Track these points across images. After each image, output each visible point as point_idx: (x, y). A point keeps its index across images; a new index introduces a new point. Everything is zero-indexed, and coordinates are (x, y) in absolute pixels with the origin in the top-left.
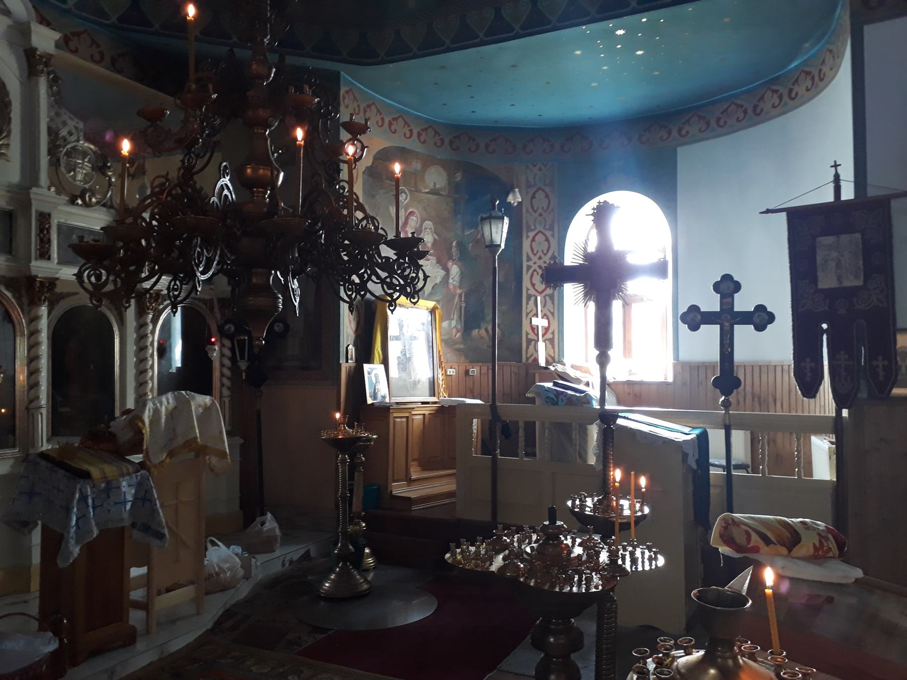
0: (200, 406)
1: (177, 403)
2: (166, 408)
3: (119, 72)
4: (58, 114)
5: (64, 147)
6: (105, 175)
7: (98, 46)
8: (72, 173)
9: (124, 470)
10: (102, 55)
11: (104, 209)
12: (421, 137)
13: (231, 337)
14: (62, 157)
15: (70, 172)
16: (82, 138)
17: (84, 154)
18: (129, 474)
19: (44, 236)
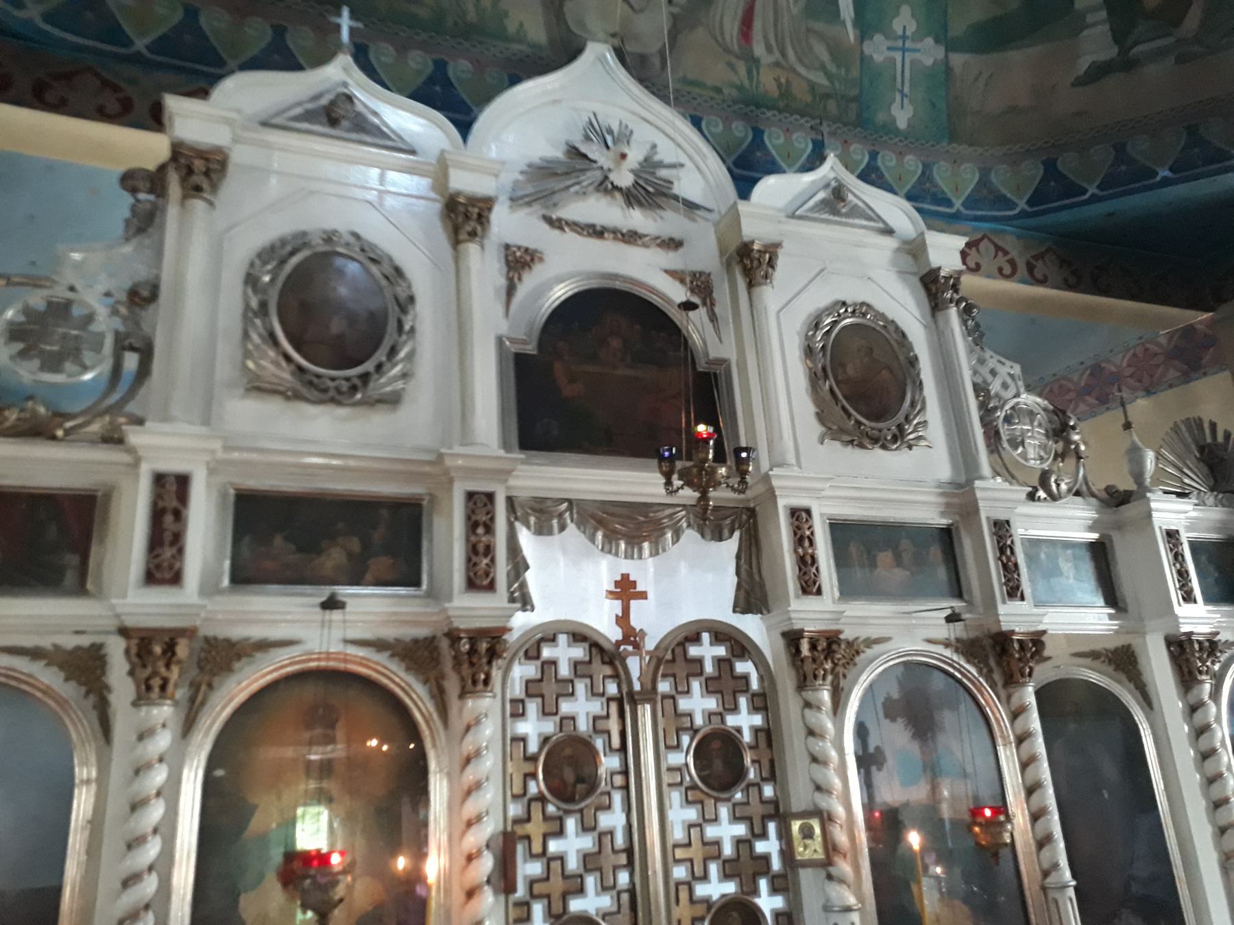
1: (231, 660)
3: (1042, 282)
4: (982, 361)
5: (1002, 408)
7: (1006, 253)
8: (1020, 450)
10: (1012, 263)
11: (1079, 499)
14: (1000, 425)
15: (1016, 448)
16: (1022, 390)
17: (1031, 414)
19: (1009, 559)
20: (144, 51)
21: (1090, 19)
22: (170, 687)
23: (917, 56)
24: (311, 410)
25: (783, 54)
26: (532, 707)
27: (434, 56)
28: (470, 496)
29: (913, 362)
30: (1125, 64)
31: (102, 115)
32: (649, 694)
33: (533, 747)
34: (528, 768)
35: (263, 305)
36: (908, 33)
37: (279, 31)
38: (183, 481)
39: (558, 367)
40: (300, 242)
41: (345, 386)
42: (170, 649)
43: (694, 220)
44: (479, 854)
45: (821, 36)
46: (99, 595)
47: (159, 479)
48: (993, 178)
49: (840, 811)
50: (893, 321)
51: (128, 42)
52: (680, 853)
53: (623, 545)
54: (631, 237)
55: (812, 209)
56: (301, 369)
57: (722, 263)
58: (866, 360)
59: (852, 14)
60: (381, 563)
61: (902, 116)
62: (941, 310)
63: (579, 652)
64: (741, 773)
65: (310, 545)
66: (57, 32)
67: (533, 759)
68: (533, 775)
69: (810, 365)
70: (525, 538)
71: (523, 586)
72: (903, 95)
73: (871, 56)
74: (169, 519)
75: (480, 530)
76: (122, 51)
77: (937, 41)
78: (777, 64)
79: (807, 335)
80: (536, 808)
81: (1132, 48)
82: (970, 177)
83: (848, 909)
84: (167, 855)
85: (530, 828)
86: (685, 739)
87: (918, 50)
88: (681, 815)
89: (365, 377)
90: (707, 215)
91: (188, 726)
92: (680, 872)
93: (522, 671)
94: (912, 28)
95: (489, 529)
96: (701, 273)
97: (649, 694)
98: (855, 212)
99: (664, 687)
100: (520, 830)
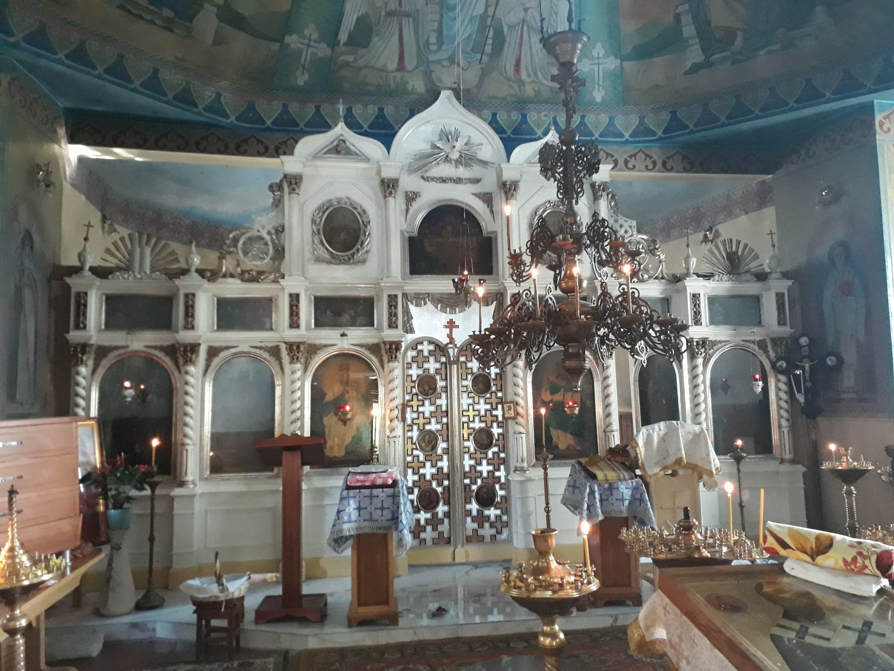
0: (689, 433)
2: (658, 434)
6: (654, 255)
9: (621, 476)
10: (654, 163)
11: (657, 281)
12: (884, 126)
13: (782, 372)
18: (625, 480)
20: (270, 125)
21: (690, 42)
22: (445, 156)
23: (606, 65)
24: (336, 267)
25: (536, 75)
26: (414, 365)
27: (379, 106)
28: (389, 296)
30: (707, 64)
31: (259, 154)
32: (457, 362)
33: (414, 378)
34: (413, 384)
35: (318, 231)
36: (601, 55)
37: (318, 108)
38: (298, 296)
39: (426, 241)
40: (328, 204)
41: (346, 258)
42: (298, 347)
43: (487, 168)
44: (394, 409)
46: (277, 331)
47: (291, 295)
49: (521, 402)
51: (264, 122)
52: (465, 413)
53: (448, 309)
54: (458, 181)
56: (331, 253)
60: (361, 319)
63: (432, 347)
64: (489, 387)
65: (338, 314)
66: (243, 124)
67: (414, 382)
68: (414, 387)
70: (412, 308)
71: (411, 325)
72: (599, 85)
74: (295, 308)
75: (393, 308)
76: (263, 127)
77: (616, 57)
78: (533, 82)
80: (415, 398)
81: (711, 56)
82: (634, 121)
83: (521, 433)
84: (302, 406)
85: (412, 403)
86: (469, 377)
88: (465, 401)
89: (353, 255)
91: (305, 370)
92: (465, 419)
93: (411, 354)
94: (602, 52)
95: (396, 307)
96: (487, 193)
97: (457, 362)
99: (462, 359)
100: (410, 404)
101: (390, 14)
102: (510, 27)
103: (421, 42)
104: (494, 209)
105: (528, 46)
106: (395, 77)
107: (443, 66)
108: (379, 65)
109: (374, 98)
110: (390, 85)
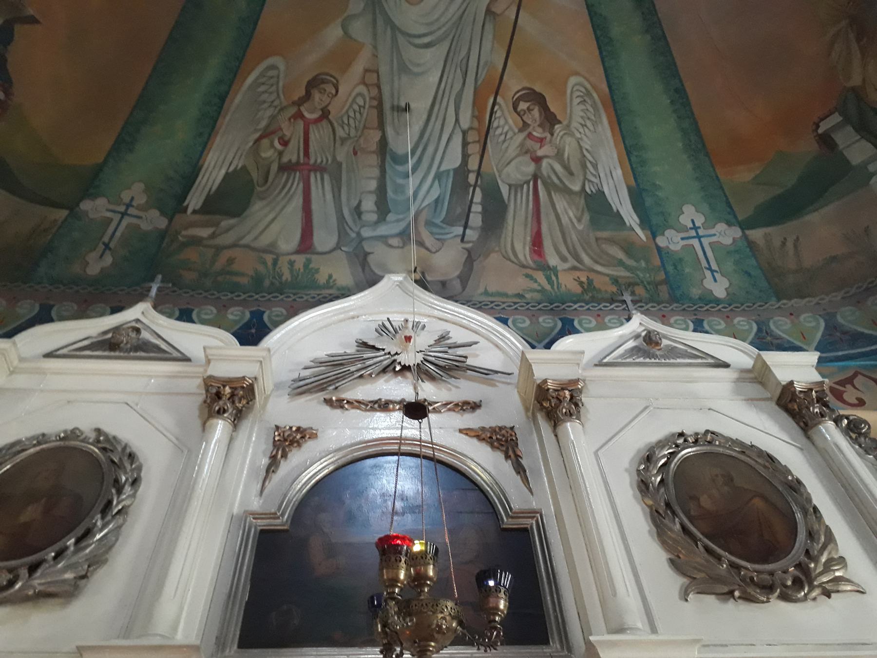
29: (796, 486)
45: (611, 241)
48: (840, 319)
50: (752, 446)
55: (622, 356)
57: (528, 417)
58: (726, 488)
59: (638, 221)
61: (719, 288)
62: (812, 428)
69: (650, 502)
73: (668, 247)
77: (729, 224)
79: (638, 471)
87: (715, 235)
90: (508, 379)
94: (700, 221)
98: (672, 352)
101: (287, 168)
102: (515, 188)
103: (346, 212)
104: (524, 462)
105: (553, 217)
106: (291, 263)
107: (391, 246)
108: (265, 241)
109: (243, 297)
110: (281, 276)
